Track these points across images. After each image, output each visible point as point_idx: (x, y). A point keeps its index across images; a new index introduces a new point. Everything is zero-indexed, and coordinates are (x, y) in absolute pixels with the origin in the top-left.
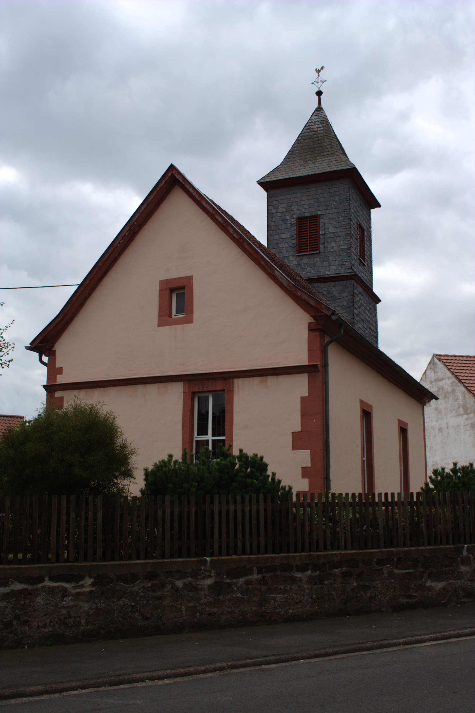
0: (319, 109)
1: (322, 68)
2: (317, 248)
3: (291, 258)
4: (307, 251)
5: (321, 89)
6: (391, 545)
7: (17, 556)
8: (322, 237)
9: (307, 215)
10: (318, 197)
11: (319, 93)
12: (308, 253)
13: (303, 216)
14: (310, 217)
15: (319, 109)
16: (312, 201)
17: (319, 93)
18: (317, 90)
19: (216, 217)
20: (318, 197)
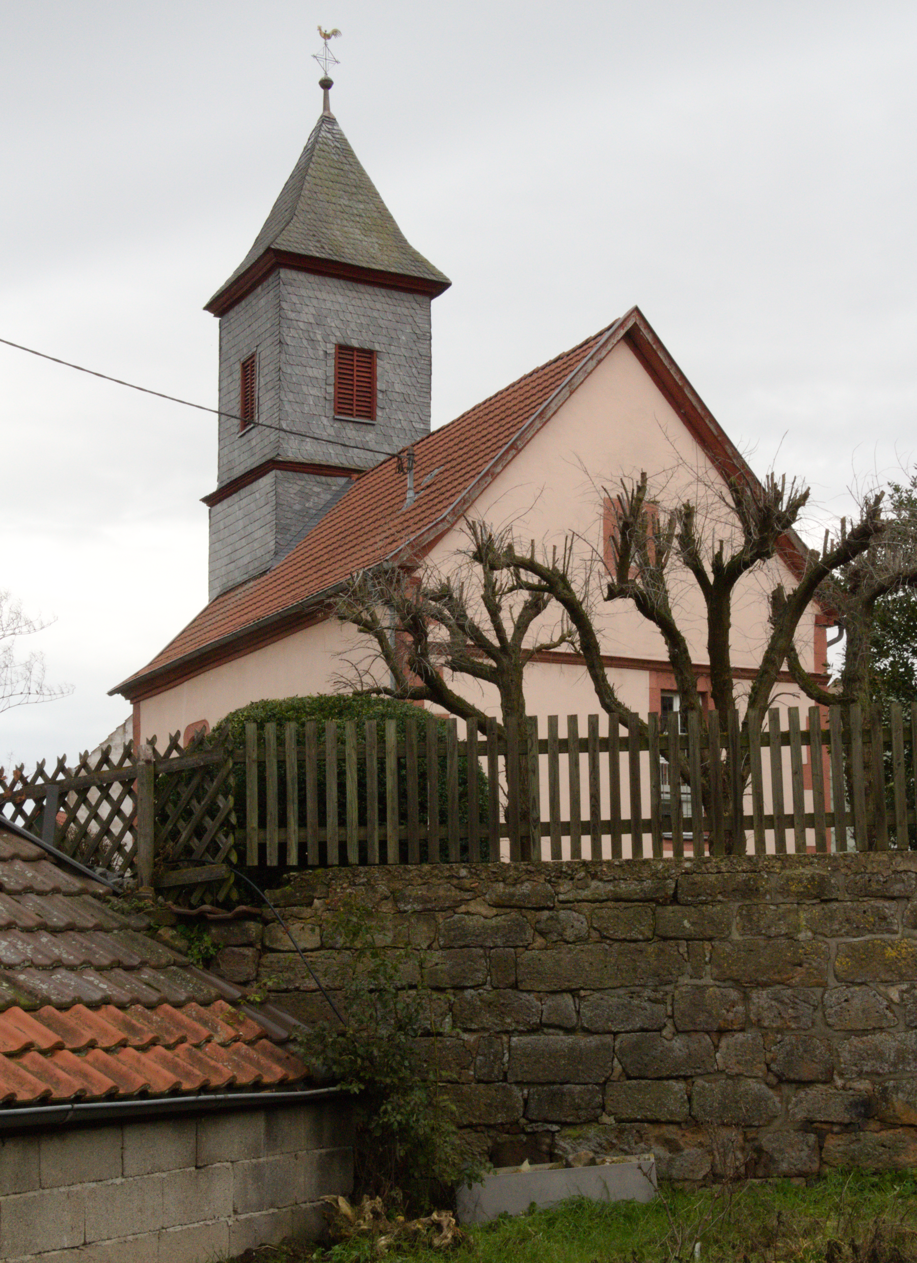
0: (327, 120)
1: (335, 33)
2: (371, 415)
3: (325, 421)
4: (351, 415)
5: (331, 76)
6: (256, 1166)
7: (825, 634)
8: (380, 396)
9: (355, 344)
10: (375, 314)
11: (326, 84)
12: (352, 419)
13: (349, 344)
14: (362, 350)
15: (327, 120)
16: (364, 320)
17: (326, 84)
18: (322, 76)
19: (707, 422)
20: (375, 314)
